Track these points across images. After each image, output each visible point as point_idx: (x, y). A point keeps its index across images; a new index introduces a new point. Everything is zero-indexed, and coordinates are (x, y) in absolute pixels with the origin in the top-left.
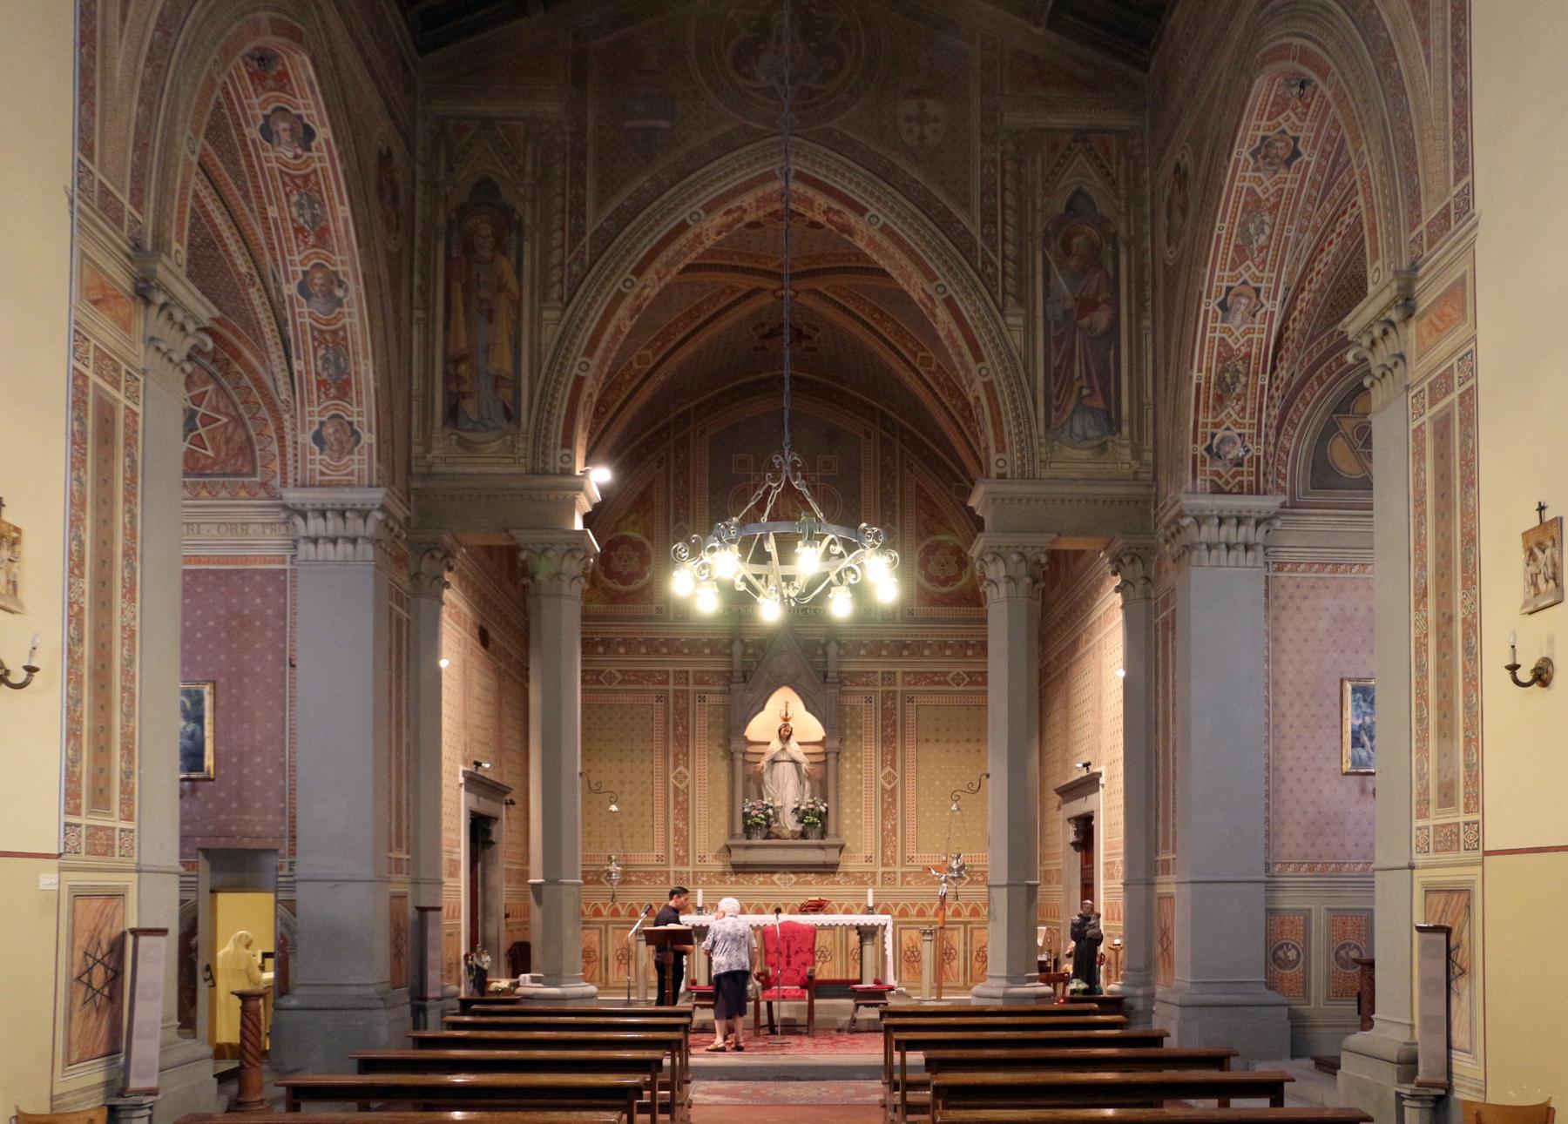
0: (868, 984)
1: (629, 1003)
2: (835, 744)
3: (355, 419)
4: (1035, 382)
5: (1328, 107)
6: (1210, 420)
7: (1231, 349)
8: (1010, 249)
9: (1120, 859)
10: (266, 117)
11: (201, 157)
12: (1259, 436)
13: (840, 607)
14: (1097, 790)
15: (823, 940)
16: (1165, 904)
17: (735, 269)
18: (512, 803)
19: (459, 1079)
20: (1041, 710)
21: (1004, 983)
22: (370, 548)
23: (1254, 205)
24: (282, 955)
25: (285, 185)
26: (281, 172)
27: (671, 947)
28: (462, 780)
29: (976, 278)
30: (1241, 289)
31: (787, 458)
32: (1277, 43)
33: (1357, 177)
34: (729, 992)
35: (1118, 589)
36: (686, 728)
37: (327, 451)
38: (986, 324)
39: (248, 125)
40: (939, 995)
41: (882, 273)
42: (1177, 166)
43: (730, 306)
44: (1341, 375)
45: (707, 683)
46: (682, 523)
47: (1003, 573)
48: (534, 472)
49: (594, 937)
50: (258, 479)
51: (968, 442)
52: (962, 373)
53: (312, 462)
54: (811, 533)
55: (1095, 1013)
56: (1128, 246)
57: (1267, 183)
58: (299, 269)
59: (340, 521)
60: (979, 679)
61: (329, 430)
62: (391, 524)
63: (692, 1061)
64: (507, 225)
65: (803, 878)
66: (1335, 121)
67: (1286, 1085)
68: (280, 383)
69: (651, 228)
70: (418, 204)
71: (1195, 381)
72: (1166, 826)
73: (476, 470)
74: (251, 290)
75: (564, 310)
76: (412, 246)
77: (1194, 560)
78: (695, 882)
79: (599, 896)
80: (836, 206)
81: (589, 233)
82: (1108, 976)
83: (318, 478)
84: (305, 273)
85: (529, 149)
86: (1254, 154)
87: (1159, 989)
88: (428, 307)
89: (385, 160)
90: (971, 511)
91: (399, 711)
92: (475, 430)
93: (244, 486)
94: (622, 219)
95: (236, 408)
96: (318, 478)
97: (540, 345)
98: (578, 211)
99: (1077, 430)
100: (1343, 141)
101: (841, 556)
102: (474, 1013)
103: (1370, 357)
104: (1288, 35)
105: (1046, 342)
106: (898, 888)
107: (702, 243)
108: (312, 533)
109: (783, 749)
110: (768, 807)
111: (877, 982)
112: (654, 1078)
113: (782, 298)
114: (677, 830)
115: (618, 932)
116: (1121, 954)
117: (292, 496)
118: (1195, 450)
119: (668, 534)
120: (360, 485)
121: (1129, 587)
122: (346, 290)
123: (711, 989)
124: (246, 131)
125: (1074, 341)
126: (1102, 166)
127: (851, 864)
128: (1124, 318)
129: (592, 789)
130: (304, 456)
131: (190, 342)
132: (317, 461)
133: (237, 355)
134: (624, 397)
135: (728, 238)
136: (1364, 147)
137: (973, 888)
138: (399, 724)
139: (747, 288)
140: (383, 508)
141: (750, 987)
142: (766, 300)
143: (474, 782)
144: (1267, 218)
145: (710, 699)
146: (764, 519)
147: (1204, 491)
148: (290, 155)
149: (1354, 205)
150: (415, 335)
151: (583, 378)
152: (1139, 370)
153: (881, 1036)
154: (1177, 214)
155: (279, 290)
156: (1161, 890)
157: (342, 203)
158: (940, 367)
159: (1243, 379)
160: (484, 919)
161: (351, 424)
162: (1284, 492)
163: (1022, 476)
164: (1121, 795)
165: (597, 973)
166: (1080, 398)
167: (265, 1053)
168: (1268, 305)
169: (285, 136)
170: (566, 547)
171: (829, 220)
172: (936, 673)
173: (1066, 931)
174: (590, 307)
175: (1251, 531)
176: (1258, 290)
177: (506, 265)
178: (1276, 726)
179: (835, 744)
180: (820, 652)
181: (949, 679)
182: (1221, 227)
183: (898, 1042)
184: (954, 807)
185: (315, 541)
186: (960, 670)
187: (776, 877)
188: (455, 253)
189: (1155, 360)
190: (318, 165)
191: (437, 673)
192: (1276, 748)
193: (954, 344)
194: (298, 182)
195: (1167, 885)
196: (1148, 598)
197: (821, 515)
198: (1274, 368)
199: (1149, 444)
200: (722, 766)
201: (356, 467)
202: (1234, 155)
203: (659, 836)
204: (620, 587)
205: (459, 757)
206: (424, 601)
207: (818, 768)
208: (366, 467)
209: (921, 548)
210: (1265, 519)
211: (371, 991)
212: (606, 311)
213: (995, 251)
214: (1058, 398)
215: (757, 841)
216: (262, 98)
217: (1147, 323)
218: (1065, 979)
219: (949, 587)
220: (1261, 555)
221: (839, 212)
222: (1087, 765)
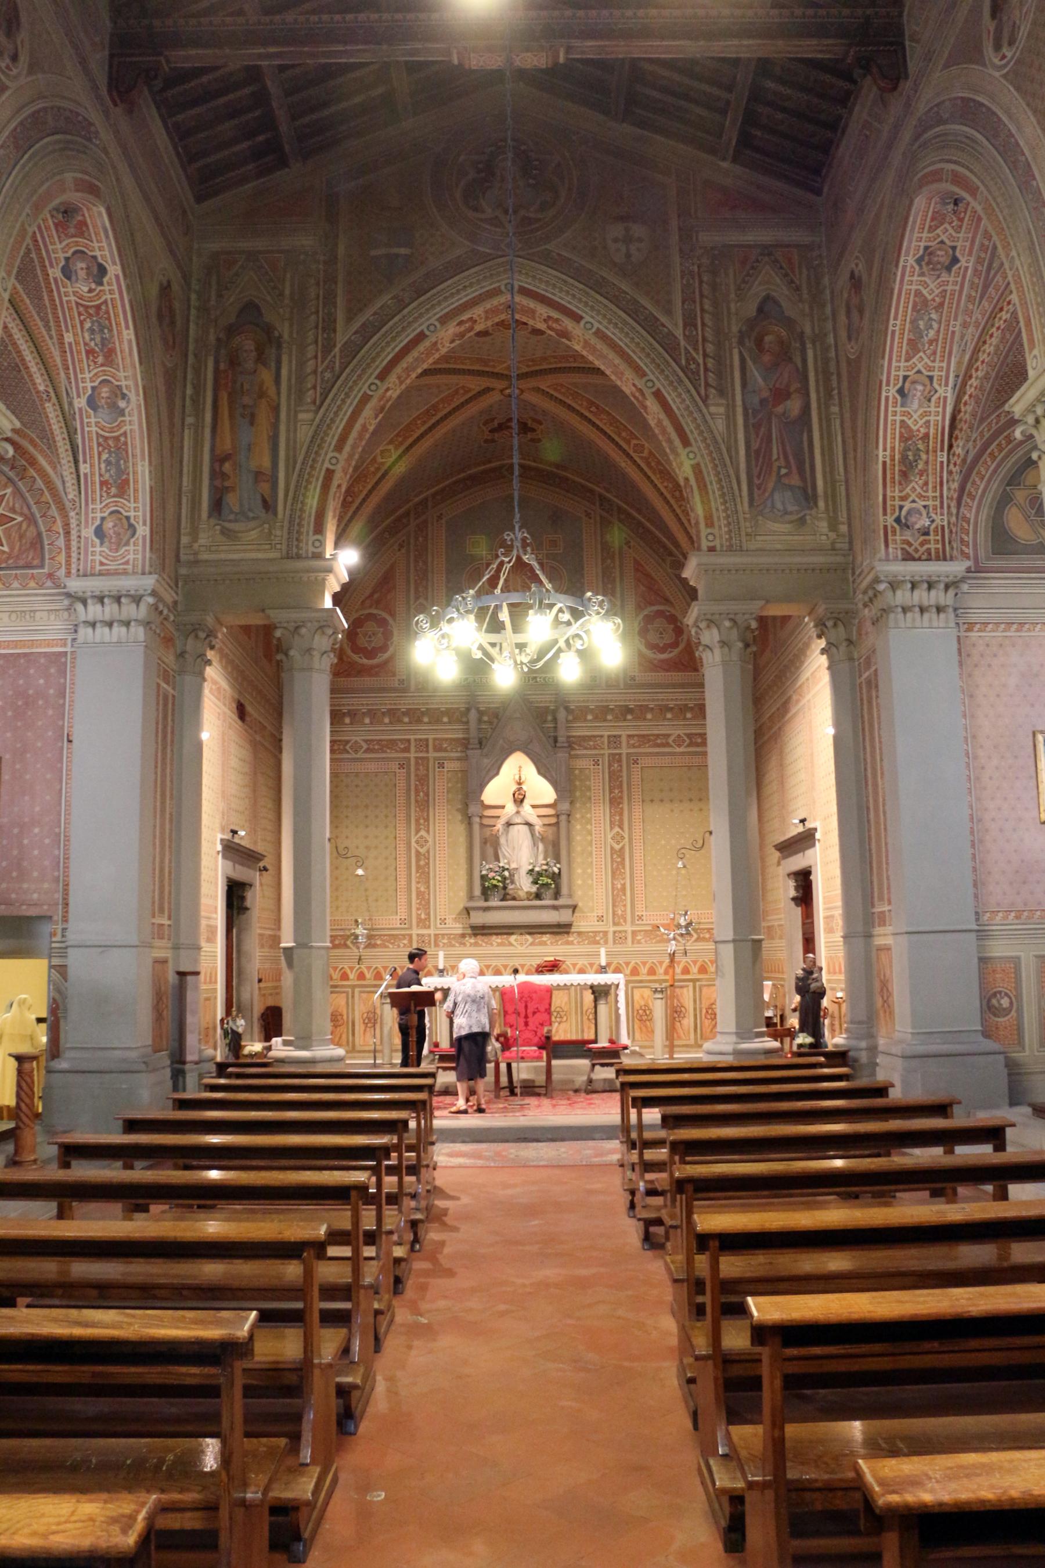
0: (603, 1043)
1: (375, 1065)
2: (565, 806)
3: (132, 514)
4: (738, 465)
5: (980, 219)
6: (897, 494)
7: (911, 430)
8: (710, 348)
9: (838, 913)
10: (67, 259)
11: (11, 295)
12: (942, 507)
13: (569, 673)
14: (814, 845)
15: (558, 1000)
16: (883, 955)
17: (470, 372)
18: (265, 869)
19: (215, 1139)
20: (757, 769)
21: (733, 1038)
22: (141, 630)
23: (921, 305)
24: (54, 1020)
25: (80, 314)
26: (77, 304)
27: (413, 1007)
28: (219, 848)
29: (681, 374)
30: (918, 377)
31: (518, 535)
32: (931, 168)
33: (1010, 278)
34: (469, 1053)
35: (823, 651)
36: (427, 795)
37: (107, 544)
39: (52, 266)
40: (671, 1053)
41: (598, 371)
42: (852, 273)
43: (462, 405)
44: (1011, 452)
45: (445, 750)
46: (421, 600)
47: (717, 638)
48: (289, 557)
49: (340, 1001)
50: (46, 570)
51: (679, 520)
52: (671, 457)
53: (93, 553)
54: (541, 603)
55: (821, 1065)
56: (814, 343)
57: (932, 286)
58: (89, 385)
59: (115, 606)
60: (699, 740)
61: (109, 525)
62: (161, 607)
63: (437, 1123)
64: (269, 342)
66: (986, 231)
67: (1008, 1130)
68: (68, 485)
69: (393, 339)
70: (192, 326)
71: (881, 459)
72: (880, 874)
73: (235, 556)
74: (47, 405)
75: (317, 412)
76: (186, 363)
77: (891, 624)
78: (436, 945)
79: (346, 958)
80: (555, 315)
81: (339, 346)
82: (833, 1031)
83: (98, 568)
84: (93, 388)
85: (288, 276)
86: (919, 261)
87: (882, 1042)
88: (199, 413)
89: (165, 289)
90: (684, 582)
91: (163, 782)
92: (236, 521)
93: (33, 577)
94: (367, 332)
95: (29, 508)
96: (98, 568)
97: (295, 442)
98: (329, 326)
99: (779, 505)
100: (995, 248)
101: (569, 624)
102: (229, 1076)
103: (1035, 432)
104: (941, 161)
105: (746, 426)
106: (629, 946)
107: (438, 350)
108: (90, 618)
109: (518, 812)
110: (504, 869)
111: (611, 1041)
112: (400, 1139)
113: (510, 396)
114: (419, 894)
115: (364, 995)
116: (844, 1006)
117: (75, 585)
118: (886, 521)
119: (408, 609)
120: (134, 573)
121: (834, 650)
122: (128, 402)
123: (453, 1051)
124: (50, 271)
125: (770, 430)
127: (584, 923)
128: (814, 405)
129: (340, 854)
132: (98, 552)
133: (33, 462)
134: (369, 487)
135: (460, 345)
136: (1014, 253)
137: (701, 945)
138: (163, 795)
139: (478, 389)
140: (154, 593)
141: (489, 1048)
142: (495, 397)
143: (231, 850)
144: (934, 316)
145: (449, 766)
146: (498, 591)
147: (896, 559)
148: (86, 289)
149: (1009, 303)
150: (186, 438)
151: (333, 471)
152: (831, 449)
153: (617, 1096)
154: (855, 314)
155: (71, 404)
156: (879, 941)
157: (127, 328)
158: (651, 453)
159: (924, 456)
160: (239, 984)
161: (128, 518)
162: (968, 558)
163: (730, 549)
164: (837, 848)
165: (344, 1036)
166: (780, 477)
167: (38, 1116)
168: (941, 391)
169: (82, 274)
170: (317, 625)
171: (549, 328)
172: (658, 736)
173: (791, 984)
174: (340, 408)
175: (942, 594)
176: (931, 378)
177: (266, 376)
178: (978, 779)
179: (565, 806)
180: (550, 718)
181: (670, 741)
182: (895, 324)
183: (634, 1099)
184: (680, 865)
185: (93, 625)
187: (513, 938)
188: (222, 366)
189: (844, 442)
190: (109, 297)
191: (199, 746)
192: (978, 799)
193: (664, 431)
194: (91, 311)
195: (884, 936)
196: (851, 659)
197: (549, 586)
198: (951, 446)
199: (843, 517)
200: (461, 829)
201: (131, 557)
202: (901, 263)
203: (402, 899)
204: (365, 661)
205: (217, 826)
206: (188, 678)
207: (551, 831)
208: (140, 556)
209: (641, 616)
210: (954, 583)
211: (133, 1055)
212: (353, 412)
213: (696, 350)
214: (759, 477)
215: (494, 902)
216: (64, 243)
217: (835, 409)
218: (791, 1034)
219: (672, 653)
220: (952, 616)
221: (557, 320)
222: (803, 821)
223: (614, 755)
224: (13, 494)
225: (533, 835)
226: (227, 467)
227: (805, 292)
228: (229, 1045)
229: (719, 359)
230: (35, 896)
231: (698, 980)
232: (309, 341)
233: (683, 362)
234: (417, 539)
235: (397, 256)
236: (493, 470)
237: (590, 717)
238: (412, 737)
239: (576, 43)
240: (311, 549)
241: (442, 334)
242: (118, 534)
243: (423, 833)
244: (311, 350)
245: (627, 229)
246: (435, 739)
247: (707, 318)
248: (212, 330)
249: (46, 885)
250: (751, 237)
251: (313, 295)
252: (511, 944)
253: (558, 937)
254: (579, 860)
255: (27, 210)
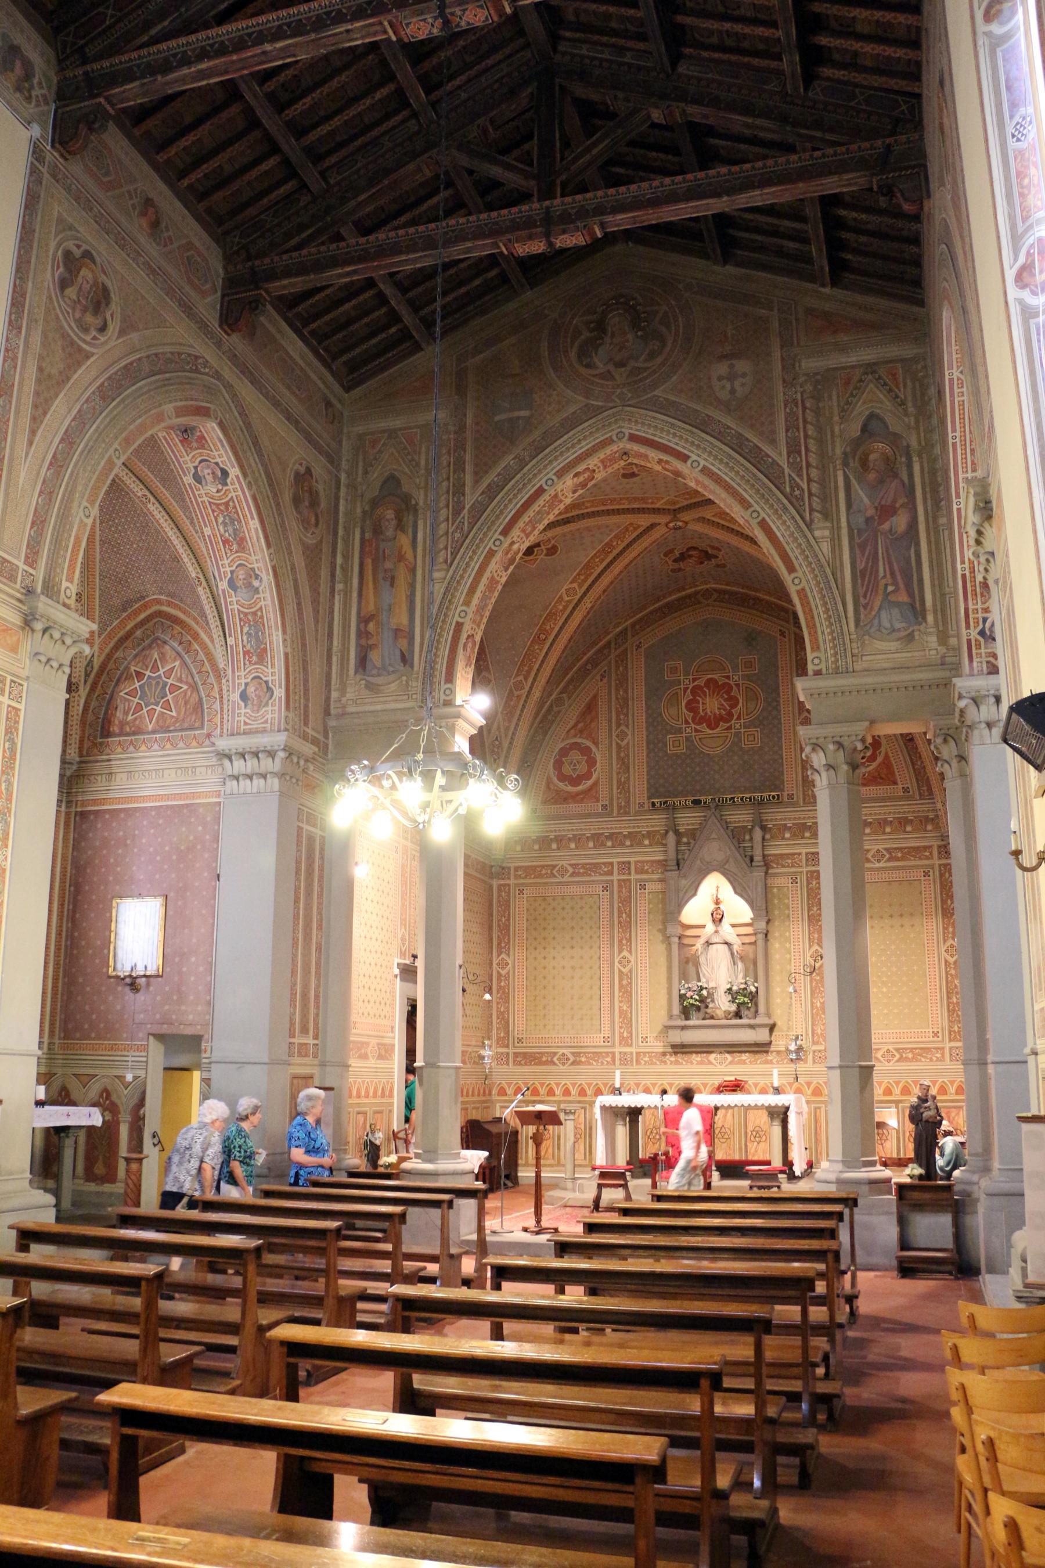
3: (270, 678)
6: (979, 606)
8: (814, 473)
21: (839, 1167)
22: (276, 781)
28: (397, 971)
29: (785, 501)
36: (629, 916)
38: (796, 539)
45: (647, 872)
56: (920, 456)
58: (228, 569)
61: (251, 689)
64: (406, 507)
65: (738, 1057)
80: (664, 457)
81: (467, 507)
84: (232, 572)
85: (423, 449)
92: (379, 675)
94: (492, 492)
98: (459, 490)
99: (886, 624)
109: (716, 932)
110: (702, 988)
114: (621, 1012)
117: (223, 744)
126: (891, 390)
128: (921, 518)
130: (234, 712)
131: (72, 651)
147: (981, 673)
161: (266, 682)
163: (837, 672)
165: (550, 1151)
166: (886, 595)
169: (210, 478)
174: (468, 565)
177: (405, 540)
180: (747, 837)
184: (791, 989)
186: (880, 847)
187: (712, 1057)
188: (367, 535)
200: (661, 948)
201: (269, 716)
203: (606, 1019)
207: (750, 949)
213: (800, 476)
214: (865, 597)
223: (813, 872)
224: (181, 666)
225: (732, 954)
226: (371, 626)
227: (910, 404)
228: (368, 1155)
229: (823, 483)
230: (191, 1017)
231: (901, 1101)
232: (441, 505)
233: (788, 489)
234: (617, 668)
235: (518, 418)
236: (689, 596)
237: (787, 835)
238: (615, 860)
239: (609, 218)
240: (443, 697)
241: (559, 487)
242: (259, 697)
243: (625, 953)
244: (443, 513)
245: (732, 366)
246: (636, 862)
247: (813, 447)
248: (359, 505)
249: (200, 1008)
250: (852, 359)
251: (445, 463)
252: (710, 1063)
253: (757, 1056)
254: (778, 978)
255: (116, 445)
